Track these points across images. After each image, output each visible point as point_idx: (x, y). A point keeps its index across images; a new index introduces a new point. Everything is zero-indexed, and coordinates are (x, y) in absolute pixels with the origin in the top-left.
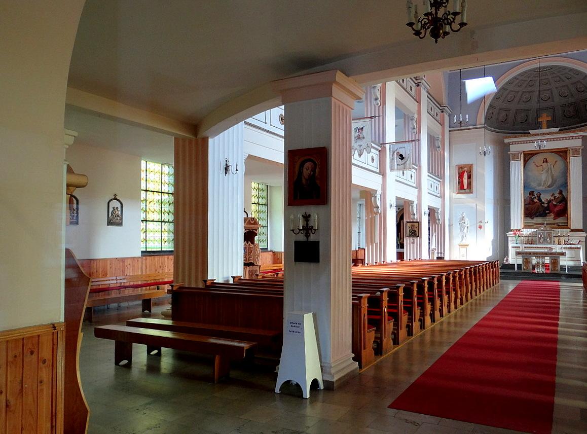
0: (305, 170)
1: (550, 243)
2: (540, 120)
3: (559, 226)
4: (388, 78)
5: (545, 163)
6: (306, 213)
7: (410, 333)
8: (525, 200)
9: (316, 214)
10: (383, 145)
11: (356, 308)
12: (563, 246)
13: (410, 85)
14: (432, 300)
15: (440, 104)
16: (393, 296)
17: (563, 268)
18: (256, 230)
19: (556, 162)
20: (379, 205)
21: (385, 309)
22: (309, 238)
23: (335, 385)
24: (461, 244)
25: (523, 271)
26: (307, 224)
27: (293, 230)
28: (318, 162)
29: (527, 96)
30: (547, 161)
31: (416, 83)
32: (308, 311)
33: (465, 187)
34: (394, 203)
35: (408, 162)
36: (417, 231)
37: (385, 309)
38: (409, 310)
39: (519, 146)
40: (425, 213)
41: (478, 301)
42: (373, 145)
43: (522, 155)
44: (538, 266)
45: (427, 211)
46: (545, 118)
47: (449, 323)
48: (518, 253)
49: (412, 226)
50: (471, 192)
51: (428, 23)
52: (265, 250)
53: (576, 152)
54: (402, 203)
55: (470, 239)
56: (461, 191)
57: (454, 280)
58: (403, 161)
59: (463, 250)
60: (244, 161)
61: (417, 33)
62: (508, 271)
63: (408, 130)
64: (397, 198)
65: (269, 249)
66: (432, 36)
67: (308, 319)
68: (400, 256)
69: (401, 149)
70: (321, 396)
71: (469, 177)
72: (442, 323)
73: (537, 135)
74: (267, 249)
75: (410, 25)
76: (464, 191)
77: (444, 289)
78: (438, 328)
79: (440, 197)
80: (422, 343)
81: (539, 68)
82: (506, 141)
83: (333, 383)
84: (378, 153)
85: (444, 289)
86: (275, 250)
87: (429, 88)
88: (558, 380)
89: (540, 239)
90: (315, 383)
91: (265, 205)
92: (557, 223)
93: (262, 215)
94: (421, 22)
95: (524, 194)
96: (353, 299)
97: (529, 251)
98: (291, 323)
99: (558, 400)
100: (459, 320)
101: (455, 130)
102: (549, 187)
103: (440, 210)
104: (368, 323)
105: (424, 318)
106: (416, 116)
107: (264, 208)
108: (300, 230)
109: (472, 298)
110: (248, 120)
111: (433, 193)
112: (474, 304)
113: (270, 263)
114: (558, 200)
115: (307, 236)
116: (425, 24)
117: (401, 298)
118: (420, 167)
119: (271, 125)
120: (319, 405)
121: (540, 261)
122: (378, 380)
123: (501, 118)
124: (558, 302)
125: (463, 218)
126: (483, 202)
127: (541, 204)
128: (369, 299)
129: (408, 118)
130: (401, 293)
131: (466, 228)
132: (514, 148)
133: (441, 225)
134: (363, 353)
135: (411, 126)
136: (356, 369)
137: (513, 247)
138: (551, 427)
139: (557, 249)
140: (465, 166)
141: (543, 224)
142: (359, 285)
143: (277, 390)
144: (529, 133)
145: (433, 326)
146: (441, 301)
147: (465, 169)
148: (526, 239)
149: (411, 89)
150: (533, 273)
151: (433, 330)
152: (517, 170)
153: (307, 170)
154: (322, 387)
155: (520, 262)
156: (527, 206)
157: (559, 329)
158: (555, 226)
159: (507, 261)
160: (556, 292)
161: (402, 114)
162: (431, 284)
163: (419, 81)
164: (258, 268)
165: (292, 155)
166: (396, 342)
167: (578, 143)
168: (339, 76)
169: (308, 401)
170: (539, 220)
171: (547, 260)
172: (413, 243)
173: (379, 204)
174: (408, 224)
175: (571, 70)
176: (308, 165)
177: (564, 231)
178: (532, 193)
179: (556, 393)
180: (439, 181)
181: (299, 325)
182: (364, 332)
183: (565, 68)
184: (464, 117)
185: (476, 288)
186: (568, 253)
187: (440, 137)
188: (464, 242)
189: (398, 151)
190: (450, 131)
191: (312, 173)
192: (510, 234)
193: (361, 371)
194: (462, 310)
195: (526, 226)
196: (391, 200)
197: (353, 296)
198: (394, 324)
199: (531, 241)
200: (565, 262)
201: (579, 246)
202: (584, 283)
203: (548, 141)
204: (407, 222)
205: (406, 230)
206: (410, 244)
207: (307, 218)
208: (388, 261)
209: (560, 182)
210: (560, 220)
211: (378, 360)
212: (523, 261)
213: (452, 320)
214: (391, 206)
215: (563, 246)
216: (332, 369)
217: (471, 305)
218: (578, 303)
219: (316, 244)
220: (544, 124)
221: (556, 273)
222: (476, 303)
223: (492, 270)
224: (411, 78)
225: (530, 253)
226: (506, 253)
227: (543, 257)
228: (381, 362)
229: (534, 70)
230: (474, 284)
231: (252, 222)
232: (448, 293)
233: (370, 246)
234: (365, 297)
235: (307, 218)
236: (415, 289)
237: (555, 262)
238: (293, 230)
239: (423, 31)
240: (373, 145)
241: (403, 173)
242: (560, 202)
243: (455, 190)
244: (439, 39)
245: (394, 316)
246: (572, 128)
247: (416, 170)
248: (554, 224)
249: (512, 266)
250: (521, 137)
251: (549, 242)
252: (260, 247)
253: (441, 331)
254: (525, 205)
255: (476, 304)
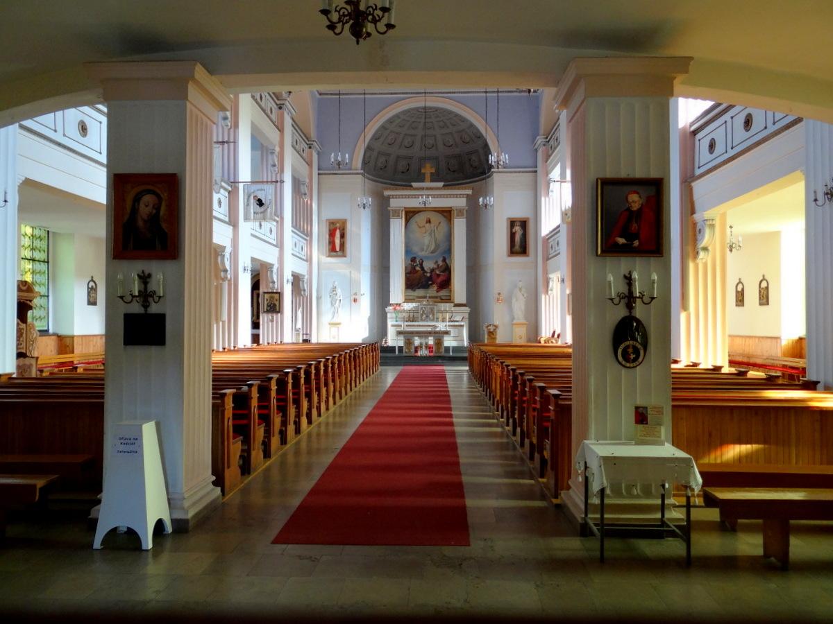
0: (142, 206)
1: (433, 320)
2: (423, 171)
3: (442, 299)
4: (245, 87)
5: (428, 224)
6: (143, 272)
7: (284, 441)
8: (406, 267)
9: (161, 274)
10: (234, 183)
11: (217, 410)
12: (448, 324)
13: (269, 105)
14: (309, 395)
15: (307, 137)
16: (264, 391)
17: (447, 349)
18: (31, 301)
19: (440, 223)
20: (228, 268)
21: (255, 410)
22: (148, 309)
23: (191, 524)
24: (332, 322)
25: (404, 354)
26: (146, 288)
27: (121, 297)
28: (164, 196)
29: (409, 140)
30: (430, 222)
31: (277, 105)
32: (148, 419)
33: (338, 249)
34: (249, 265)
35: (269, 210)
36: (278, 305)
37: (255, 410)
38: (283, 409)
39: (401, 200)
40: (288, 281)
41: (357, 393)
42: (223, 184)
43: (404, 213)
44: (421, 347)
45: (291, 278)
46: (428, 170)
47: (327, 424)
48: (399, 333)
49: (272, 297)
50: (344, 256)
51: (346, 16)
52: (44, 333)
53: (460, 212)
54: (258, 267)
55: (343, 315)
56: (332, 254)
57: (333, 368)
58: (262, 209)
59: (334, 329)
60: (17, 188)
61: (332, 27)
62: (387, 355)
63: (267, 168)
64: (253, 260)
65: (51, 331)
66: (353, 34)
67: (149, 431)
68: (255, 339)
69: (259, 192)
70: (168, 544)
71: (343, 236)
72: (319, 425)
73: (422, 189)
74: (47, 331)
75: (325, 12)
76: (335, 254)
77: (322, 379)
78: (315, 431)
79: (306, 261)
80: (297, 452)
81: (425, 108)
82: (386, 193)
83: (186, 522)
84: (227, 194)
85: (322, 379)
86: (64, 331)
87: (294, 113)
88: (465, 479)
89: (422, 315)
90: (160, 524)
91: (44, 262)
92: (440, 297)
93: (39, 278)
94: (339, 12)
95: (405, 260)
96: (213, 398)
97: (411, 330)
98: (120, 439)
99: (470, 502)
100: (337, 419)
101: (325, 174)
102: (432, 253)
103: (306, 277)
104: (234, 432)
105: (299, 419)
106: (277, 149)
107: (43, 267)
108: (134, 297)
109: (351, 390)
110: (25, 123)
111: (298, 254)
112: (353, 398)
113: (53, 353)
114: (442, 269)
115: (146, 305)
116: (344, 15)
117: (273, 394)
118: (282, 219)
119: (64, 135)
120: (165, 557)
121: (424, 341)
122: (245, 508)
123: (379, 165)
124: (446, 389)
125: (334, 289)
126: (359, 270)
127: (424, 273)
128: (235, 396)
129: (267, 151)
130: (274, 387)
131: (338, 301)
132: (394, 203)
133: (307, 297)
134: (228, 473)
135: (270, 162)
136: (218, 497)
137: (393, 326)
138: (468, 535)
139: (441, 326)
140: (338, 221)
141: (425, 297)
142: (224, 378)
143: (97, 544)
144: (411, 186)
145: (309, 429)
146: (319, 395)
147: (338, 225)
148: (405, 315)
149: (271, 112)
150: (416, 356)
151: (309, 435)
152: (397, 229)
153: (147, 206)
154: (169, 528)
155: (401, 343)
156: (408, 275)
157: (454, 420)
158: (439, 300)
159: (386, 343)
160: (442, 378)
161: (259, 145)
162: (296, 377)
163: (281, 102)
164: (33, 362)
165: (120, 183)
166: (267, 454)
167: (461, 203)
168: (200, 72)
169: (150, 555)
170: (420, 292)
171: (431, 341)
172: (272, 321)
173: (228, 266)
174: (266, 295)
175: (457, 115)
176: (147, 198)
177: (448, 306)
178: (413, 260)
179: (466, 495)
180: (306, 240)
181: (135, 441)
182: (228, 444)
183: (450, 112)
184: (343, 157)
185: (355, 377)
186: (452, 330)
187: (307, 180)
188: (336, 320)
189: (255, 194)
190: (319, 174)
191: (154, 211)
192: (390, 309)
193: (224, 500)
194: (341, 406)
195: (407, 300)
196: (244, 261)
197: (213, 394)
198: (265, 430)
199: (412, 318)
200: (449, 342)
201: (462, 323)
202: (470, 366)
203: (434, 198)
204: (265, 293)
205: (264, 305)
206: (267, 322)
207: (145, 278)
208: (240, 345)
209: (443, 247)
210: (443, 293)
211: (246, 482)
212: (406, 343)
213: (331, 420)
214: (245, 270)
215: (448, 324)
216: (184, 501)
217: (351, 400)
218: (460, 389)
219: (161, 318)
220: (428, 176)
221: (443, 357)
222: (355, 397)
223: (371, 354)
224: (269, 94)
225: (412, 333)
226: (383, 332)
227: (427, 337)
228: (249, 483)
229: (417, 109)
230: (354, 371)
231: (24, 288)
232: (326, 385)
233: (215, 325)
234: (230, 394)
235: (145, 278)
236: (290, 381)
237: (439, 342)
238: (121, 297)
239: (339, 26)
240: (223, 184)
241: (261, 225)
242: (443, 271)
243: (325, 251)
244: (361, 40)
245: (265, 419)
246: (458, 184)
247: (277, 222)
248: (436, 297)
249: (392, 349)
250: (396, 189)
251: (432, 318)
252: (37, 329)
253: (318, 435)
254: (406, 274)
255: (355, 399)
